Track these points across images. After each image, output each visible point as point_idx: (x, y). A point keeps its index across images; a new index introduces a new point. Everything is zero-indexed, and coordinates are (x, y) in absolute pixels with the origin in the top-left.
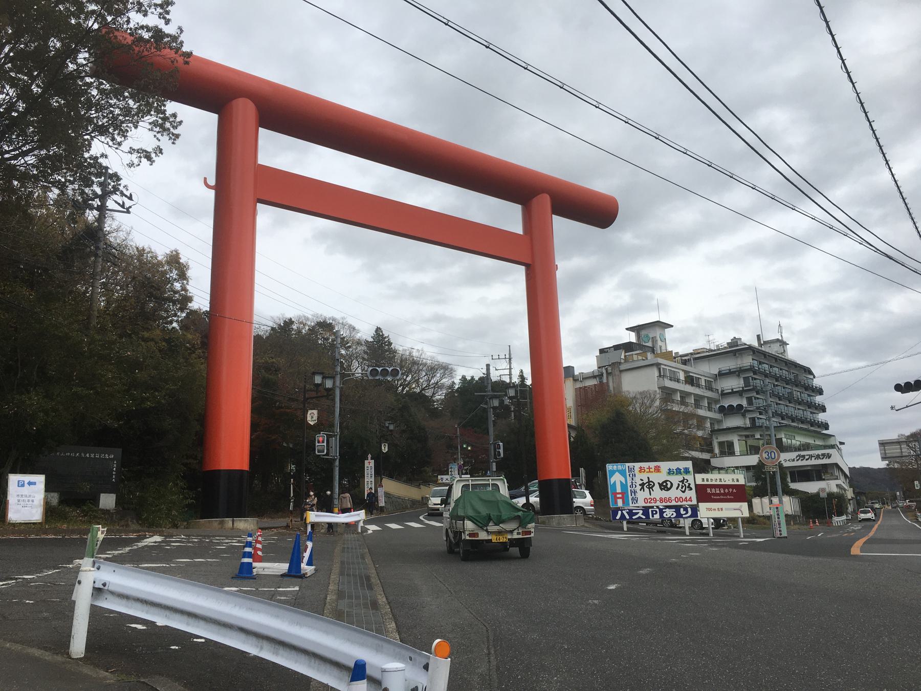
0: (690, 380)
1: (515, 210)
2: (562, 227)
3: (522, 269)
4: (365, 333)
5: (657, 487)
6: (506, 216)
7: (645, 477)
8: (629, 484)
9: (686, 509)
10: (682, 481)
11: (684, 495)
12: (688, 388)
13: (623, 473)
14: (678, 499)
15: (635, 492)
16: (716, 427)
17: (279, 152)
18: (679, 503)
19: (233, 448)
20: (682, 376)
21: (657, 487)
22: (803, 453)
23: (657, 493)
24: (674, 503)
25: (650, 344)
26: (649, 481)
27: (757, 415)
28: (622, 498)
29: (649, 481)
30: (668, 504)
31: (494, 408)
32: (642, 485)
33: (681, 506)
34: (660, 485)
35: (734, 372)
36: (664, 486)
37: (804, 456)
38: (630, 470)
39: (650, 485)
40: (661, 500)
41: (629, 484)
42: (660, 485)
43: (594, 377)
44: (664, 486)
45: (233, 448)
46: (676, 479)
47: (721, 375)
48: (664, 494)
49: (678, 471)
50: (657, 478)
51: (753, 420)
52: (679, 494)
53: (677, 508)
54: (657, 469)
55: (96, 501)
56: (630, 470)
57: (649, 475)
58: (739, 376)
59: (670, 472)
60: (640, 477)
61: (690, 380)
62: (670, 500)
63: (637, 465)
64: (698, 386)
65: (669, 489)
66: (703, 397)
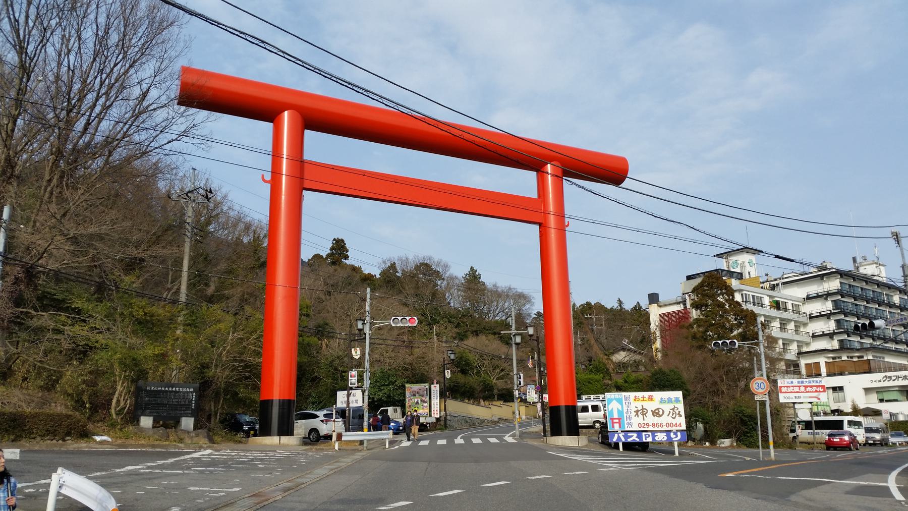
0: (777, 305)
1: (531, 176)
2: (572, 189)
3: (537, 227)
4: (459, 271)
5: (650, 414)
6: (521, 183)
7: (639, 405)
8: (625, 411)
9: (675, 434)
10: (673, 409)
11: (674, 422)
12: (774, 313)
13: (619, 401)
14: (668, 425)
15: (630, 418)
16: (805, 349)
17: (321, 147)
18: (670, 428)
19: (279, 384)
20: (766, 301)
21: (650, 414)
22: (889, 374)
23: (650, 419)
24: (665, 428)
25: (738, 270)
26: (643, 409)
27: (845, 337)
28: (619, 423)
29: (643, 409)
30: (660, 429)
31: (517, 344)
32: (637, 412)
33: (670, 431)
34: (653, 412)
35: (822, 296)
36: (656, 413)
37: (890, 377)
38: (626, 399)
39: (644, 412)
40: (653, 425)
41: (625, 411)
42: (653, 412)
43: (679, 303)
44: (656, 413)
45: (279, 384)
46: (667, 407)
47: (809, 298)
48: (656, 420)
49: (670, 400)
50: (650, 406)
51: (841, 341)
52: (669, 420)
53: (668, 432)
54: (651, 398)
55: (178, 422)
56: (626, 399)
57: (644, 403)
58: (826, 299)
59: (662, 401)
60: (635, 405)
61: (777, 305)
62: (661, 425)
63: (632, 395)
64: (786, 310)
65: (660, 416)
66: (789, 321)
